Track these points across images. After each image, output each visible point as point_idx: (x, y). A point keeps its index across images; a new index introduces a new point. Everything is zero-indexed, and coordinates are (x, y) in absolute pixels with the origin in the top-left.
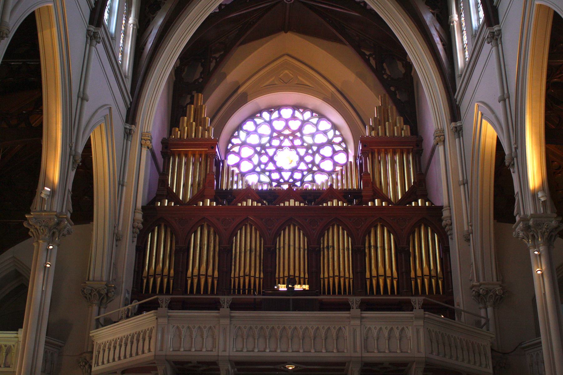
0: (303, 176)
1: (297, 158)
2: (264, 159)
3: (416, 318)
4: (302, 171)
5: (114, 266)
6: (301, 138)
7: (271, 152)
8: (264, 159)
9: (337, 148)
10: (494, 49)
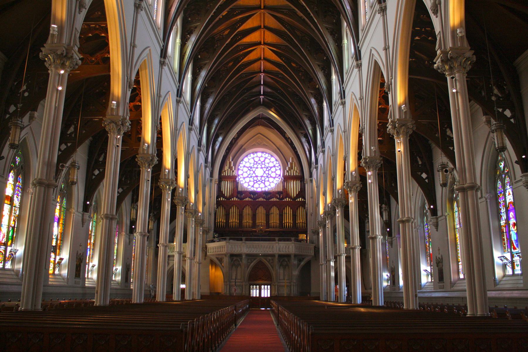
0: (265, 179)
1: (263, 172)
2: (252, 172)
3: (293, 243)
4: (264, 177)
5: (209, 223)
6: (264, 164)
7: (254, 169)
8: (252, 172)
9: (277, 168)
10: (381, 17)
